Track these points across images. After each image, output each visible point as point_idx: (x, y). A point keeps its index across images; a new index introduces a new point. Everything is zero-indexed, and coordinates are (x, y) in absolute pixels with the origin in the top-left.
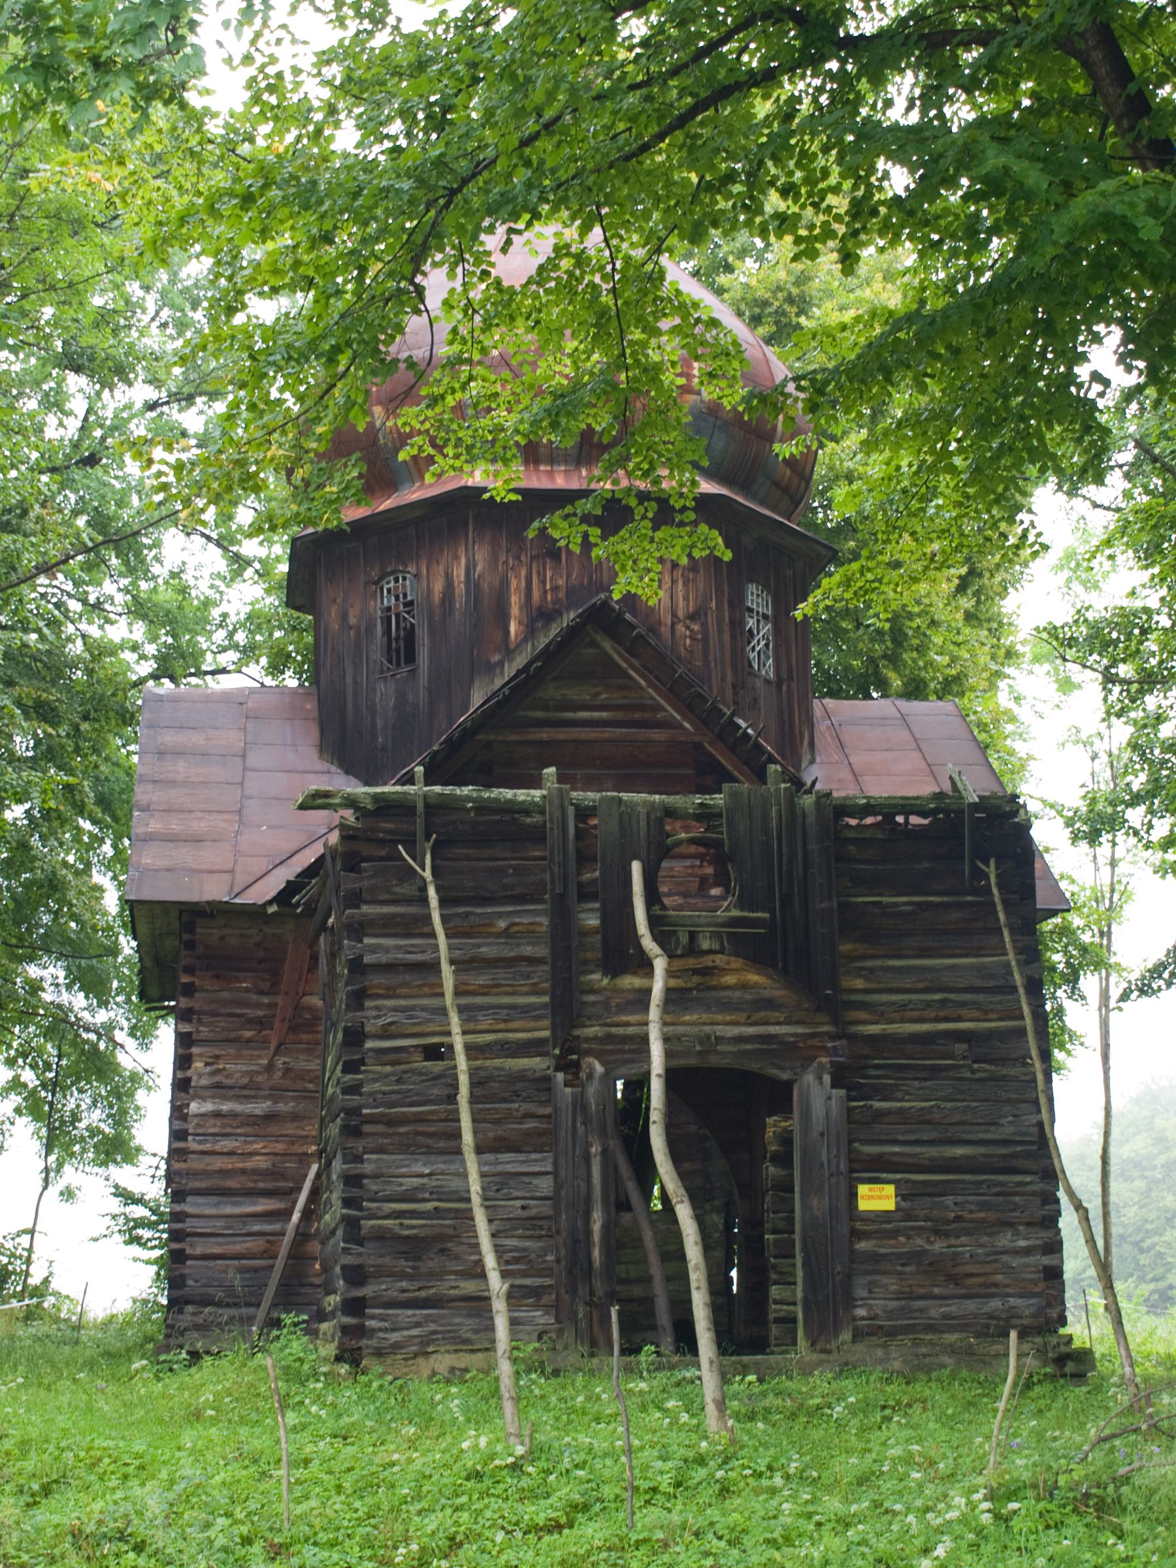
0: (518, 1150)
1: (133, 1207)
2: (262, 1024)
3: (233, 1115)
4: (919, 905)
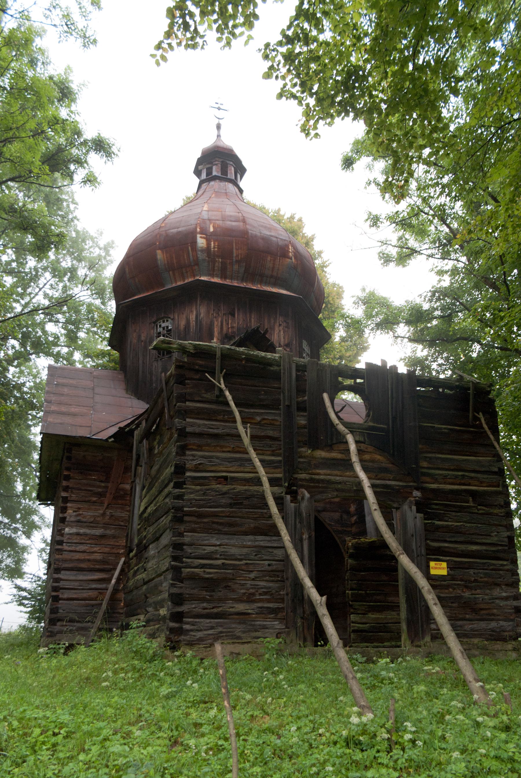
0: (266, 535)
1: (22, 592)
2: (101, 495)
3: (85, 535)
4: (450, 429)
